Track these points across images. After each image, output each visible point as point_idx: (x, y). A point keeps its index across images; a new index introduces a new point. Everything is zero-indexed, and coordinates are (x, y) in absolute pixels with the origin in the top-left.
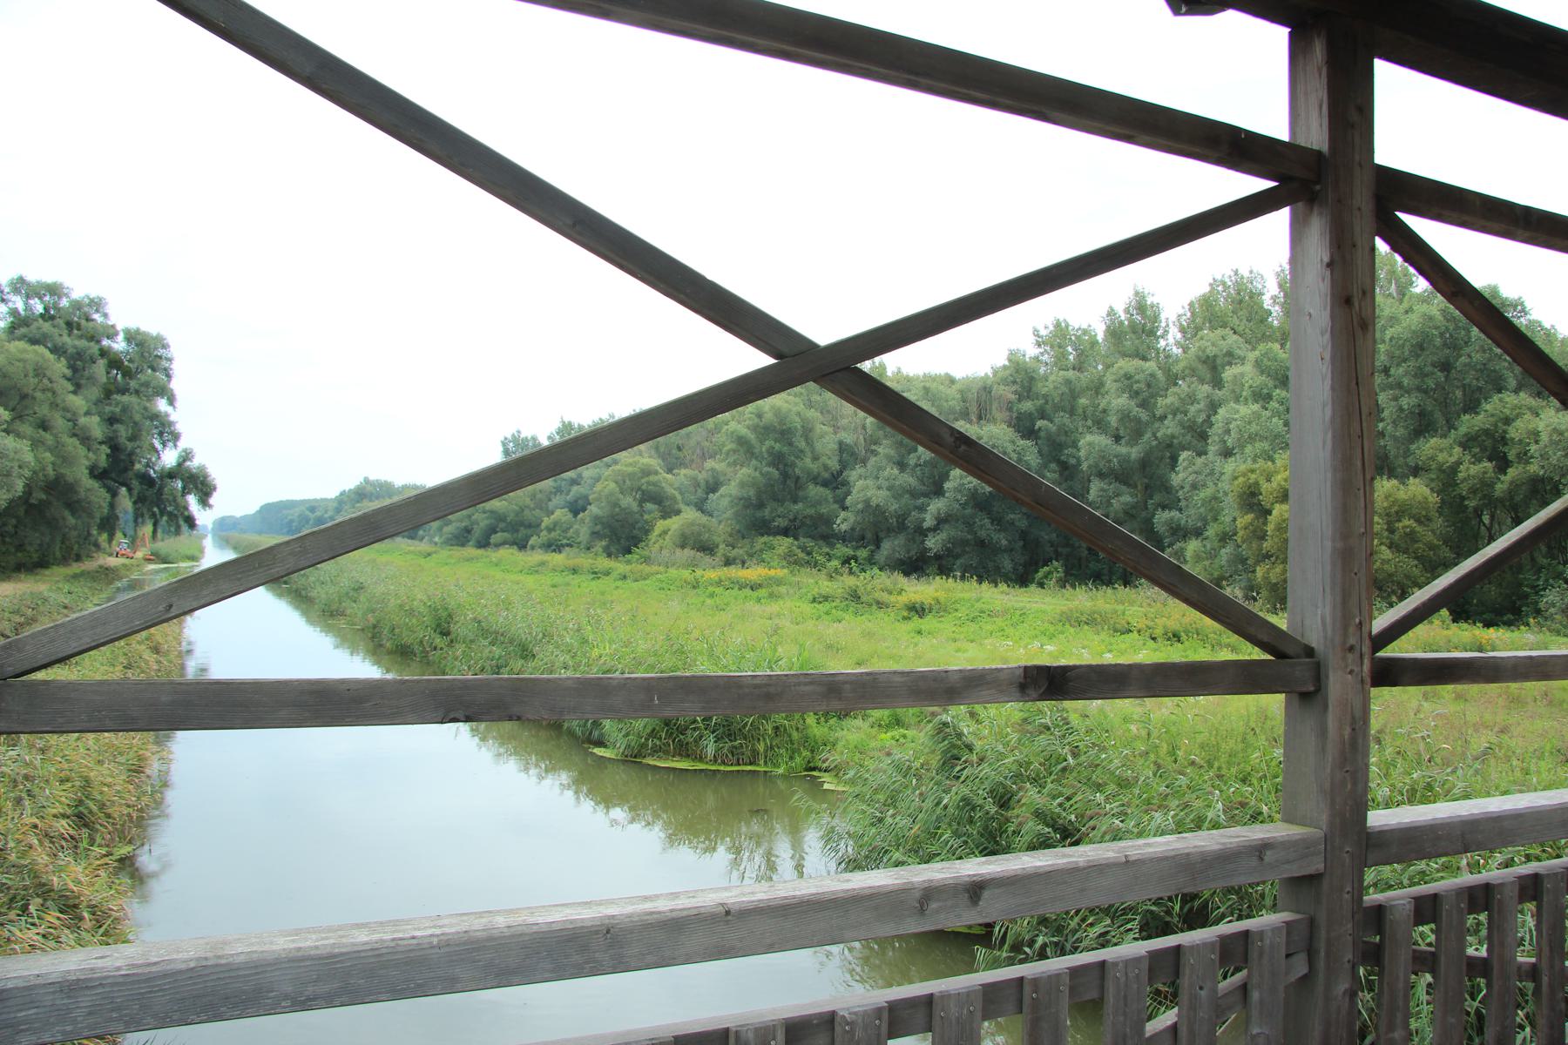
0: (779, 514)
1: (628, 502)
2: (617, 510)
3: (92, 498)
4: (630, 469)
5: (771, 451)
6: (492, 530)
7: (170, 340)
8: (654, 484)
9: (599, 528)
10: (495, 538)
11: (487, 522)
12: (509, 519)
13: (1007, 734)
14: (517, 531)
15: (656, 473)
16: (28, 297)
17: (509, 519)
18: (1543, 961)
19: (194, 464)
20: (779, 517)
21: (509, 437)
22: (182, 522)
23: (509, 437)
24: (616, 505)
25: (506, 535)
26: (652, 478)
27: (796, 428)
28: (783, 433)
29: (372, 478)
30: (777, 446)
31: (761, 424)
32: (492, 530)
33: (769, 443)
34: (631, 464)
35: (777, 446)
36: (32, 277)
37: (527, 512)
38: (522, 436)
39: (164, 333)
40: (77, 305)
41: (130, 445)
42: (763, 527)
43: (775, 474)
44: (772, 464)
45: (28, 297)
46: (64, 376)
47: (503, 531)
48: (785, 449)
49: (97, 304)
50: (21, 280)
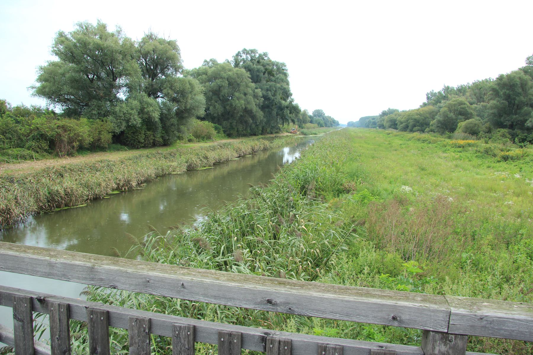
0: (507, 120)
1: (452, 115)
2: (446, 118)
3: (257, 114)
4: (454, 103)
5: (504, 94)
6: (414, 126)
7: (286, 64)
8: (463, 108)
9: (439, 125)
10: (415, 129)
11: (413, 123)
12: (420, 122)
13: (238, 198)
14: (423, 126)
15: (465, 104)
16: (247, 54)
17: (420, 122)
18: (315, 336)
19: (294, 103)
20: (507, 121)
21: (429, 92)
22: (290, 121)
23: (429, 92)
24: (447, 116)
25: (419, 128)
26: (463, 106)
27: (517, 84)
28: (511, 86)
29: (391, 108)
30: (507, 92)
31: (502, 83)
32: (414, 126)
33: (503, 91)
34: (454, 101)
35: (507, 92)
36: (248, 49)
37: (427, 119)
38: (434, 92)
39: (285, 62)
40: (260, 55)
41: (273, 98)
42: (501, 125)
43: (507, 103)
44: (506, 100)
45: (247, 54)
46: (248, 77)
47: (418, 126)
48: (511, 93)
49: (265, 54)
50: (245, 50)
